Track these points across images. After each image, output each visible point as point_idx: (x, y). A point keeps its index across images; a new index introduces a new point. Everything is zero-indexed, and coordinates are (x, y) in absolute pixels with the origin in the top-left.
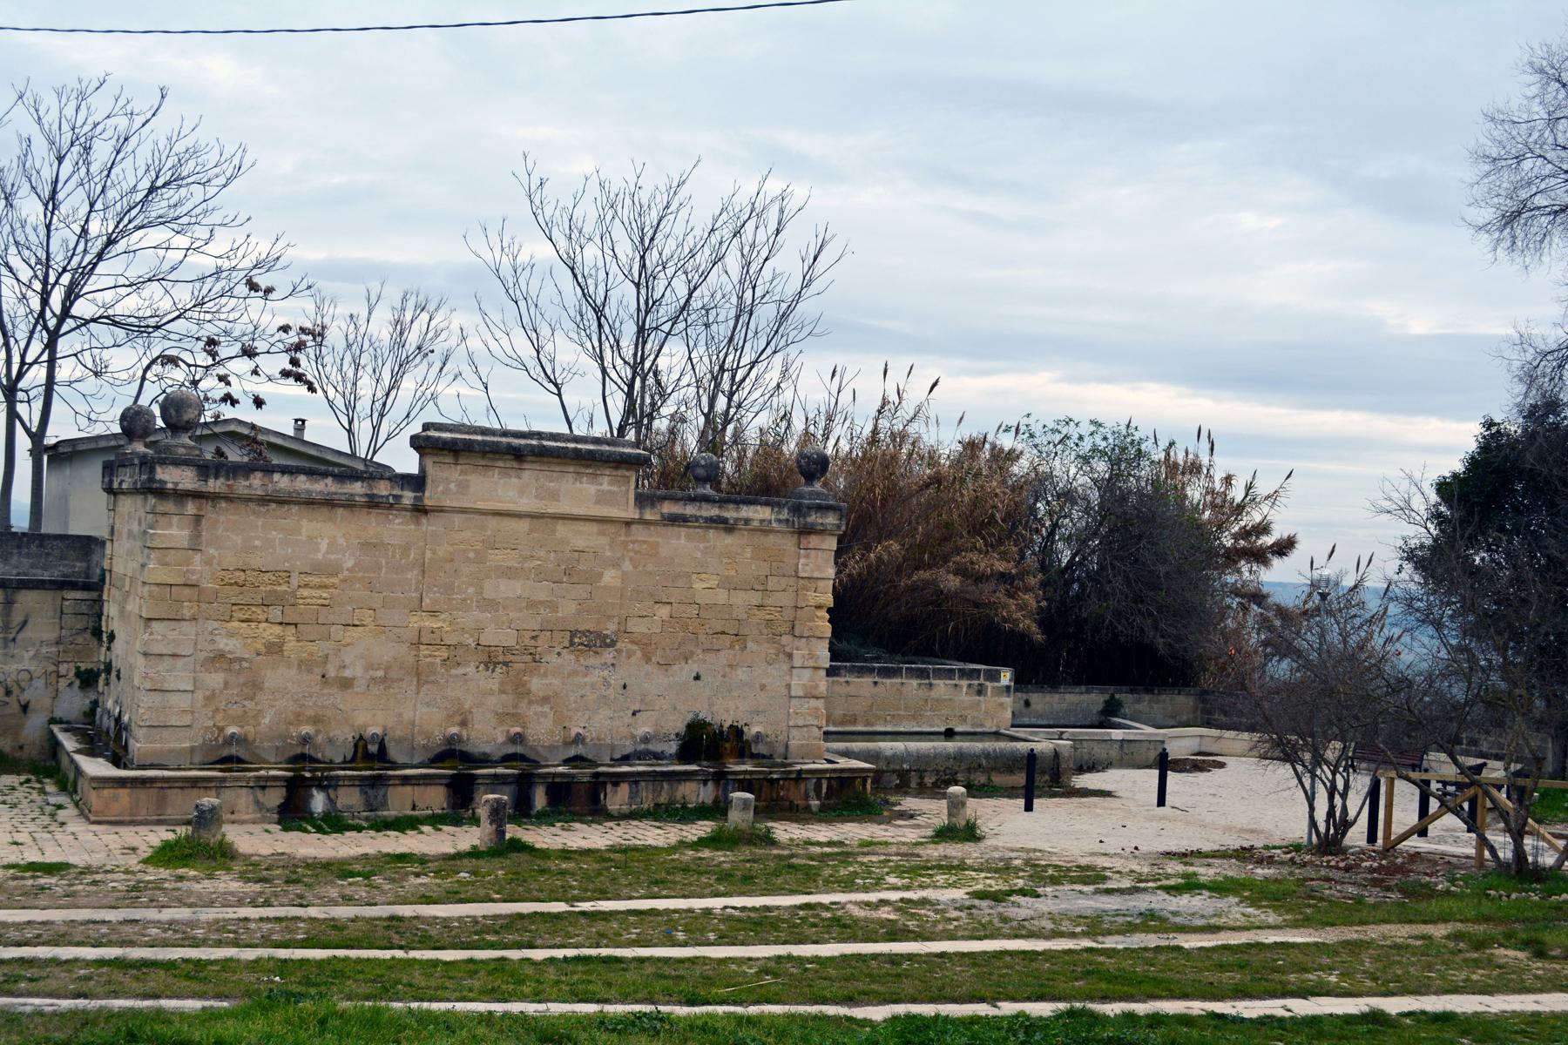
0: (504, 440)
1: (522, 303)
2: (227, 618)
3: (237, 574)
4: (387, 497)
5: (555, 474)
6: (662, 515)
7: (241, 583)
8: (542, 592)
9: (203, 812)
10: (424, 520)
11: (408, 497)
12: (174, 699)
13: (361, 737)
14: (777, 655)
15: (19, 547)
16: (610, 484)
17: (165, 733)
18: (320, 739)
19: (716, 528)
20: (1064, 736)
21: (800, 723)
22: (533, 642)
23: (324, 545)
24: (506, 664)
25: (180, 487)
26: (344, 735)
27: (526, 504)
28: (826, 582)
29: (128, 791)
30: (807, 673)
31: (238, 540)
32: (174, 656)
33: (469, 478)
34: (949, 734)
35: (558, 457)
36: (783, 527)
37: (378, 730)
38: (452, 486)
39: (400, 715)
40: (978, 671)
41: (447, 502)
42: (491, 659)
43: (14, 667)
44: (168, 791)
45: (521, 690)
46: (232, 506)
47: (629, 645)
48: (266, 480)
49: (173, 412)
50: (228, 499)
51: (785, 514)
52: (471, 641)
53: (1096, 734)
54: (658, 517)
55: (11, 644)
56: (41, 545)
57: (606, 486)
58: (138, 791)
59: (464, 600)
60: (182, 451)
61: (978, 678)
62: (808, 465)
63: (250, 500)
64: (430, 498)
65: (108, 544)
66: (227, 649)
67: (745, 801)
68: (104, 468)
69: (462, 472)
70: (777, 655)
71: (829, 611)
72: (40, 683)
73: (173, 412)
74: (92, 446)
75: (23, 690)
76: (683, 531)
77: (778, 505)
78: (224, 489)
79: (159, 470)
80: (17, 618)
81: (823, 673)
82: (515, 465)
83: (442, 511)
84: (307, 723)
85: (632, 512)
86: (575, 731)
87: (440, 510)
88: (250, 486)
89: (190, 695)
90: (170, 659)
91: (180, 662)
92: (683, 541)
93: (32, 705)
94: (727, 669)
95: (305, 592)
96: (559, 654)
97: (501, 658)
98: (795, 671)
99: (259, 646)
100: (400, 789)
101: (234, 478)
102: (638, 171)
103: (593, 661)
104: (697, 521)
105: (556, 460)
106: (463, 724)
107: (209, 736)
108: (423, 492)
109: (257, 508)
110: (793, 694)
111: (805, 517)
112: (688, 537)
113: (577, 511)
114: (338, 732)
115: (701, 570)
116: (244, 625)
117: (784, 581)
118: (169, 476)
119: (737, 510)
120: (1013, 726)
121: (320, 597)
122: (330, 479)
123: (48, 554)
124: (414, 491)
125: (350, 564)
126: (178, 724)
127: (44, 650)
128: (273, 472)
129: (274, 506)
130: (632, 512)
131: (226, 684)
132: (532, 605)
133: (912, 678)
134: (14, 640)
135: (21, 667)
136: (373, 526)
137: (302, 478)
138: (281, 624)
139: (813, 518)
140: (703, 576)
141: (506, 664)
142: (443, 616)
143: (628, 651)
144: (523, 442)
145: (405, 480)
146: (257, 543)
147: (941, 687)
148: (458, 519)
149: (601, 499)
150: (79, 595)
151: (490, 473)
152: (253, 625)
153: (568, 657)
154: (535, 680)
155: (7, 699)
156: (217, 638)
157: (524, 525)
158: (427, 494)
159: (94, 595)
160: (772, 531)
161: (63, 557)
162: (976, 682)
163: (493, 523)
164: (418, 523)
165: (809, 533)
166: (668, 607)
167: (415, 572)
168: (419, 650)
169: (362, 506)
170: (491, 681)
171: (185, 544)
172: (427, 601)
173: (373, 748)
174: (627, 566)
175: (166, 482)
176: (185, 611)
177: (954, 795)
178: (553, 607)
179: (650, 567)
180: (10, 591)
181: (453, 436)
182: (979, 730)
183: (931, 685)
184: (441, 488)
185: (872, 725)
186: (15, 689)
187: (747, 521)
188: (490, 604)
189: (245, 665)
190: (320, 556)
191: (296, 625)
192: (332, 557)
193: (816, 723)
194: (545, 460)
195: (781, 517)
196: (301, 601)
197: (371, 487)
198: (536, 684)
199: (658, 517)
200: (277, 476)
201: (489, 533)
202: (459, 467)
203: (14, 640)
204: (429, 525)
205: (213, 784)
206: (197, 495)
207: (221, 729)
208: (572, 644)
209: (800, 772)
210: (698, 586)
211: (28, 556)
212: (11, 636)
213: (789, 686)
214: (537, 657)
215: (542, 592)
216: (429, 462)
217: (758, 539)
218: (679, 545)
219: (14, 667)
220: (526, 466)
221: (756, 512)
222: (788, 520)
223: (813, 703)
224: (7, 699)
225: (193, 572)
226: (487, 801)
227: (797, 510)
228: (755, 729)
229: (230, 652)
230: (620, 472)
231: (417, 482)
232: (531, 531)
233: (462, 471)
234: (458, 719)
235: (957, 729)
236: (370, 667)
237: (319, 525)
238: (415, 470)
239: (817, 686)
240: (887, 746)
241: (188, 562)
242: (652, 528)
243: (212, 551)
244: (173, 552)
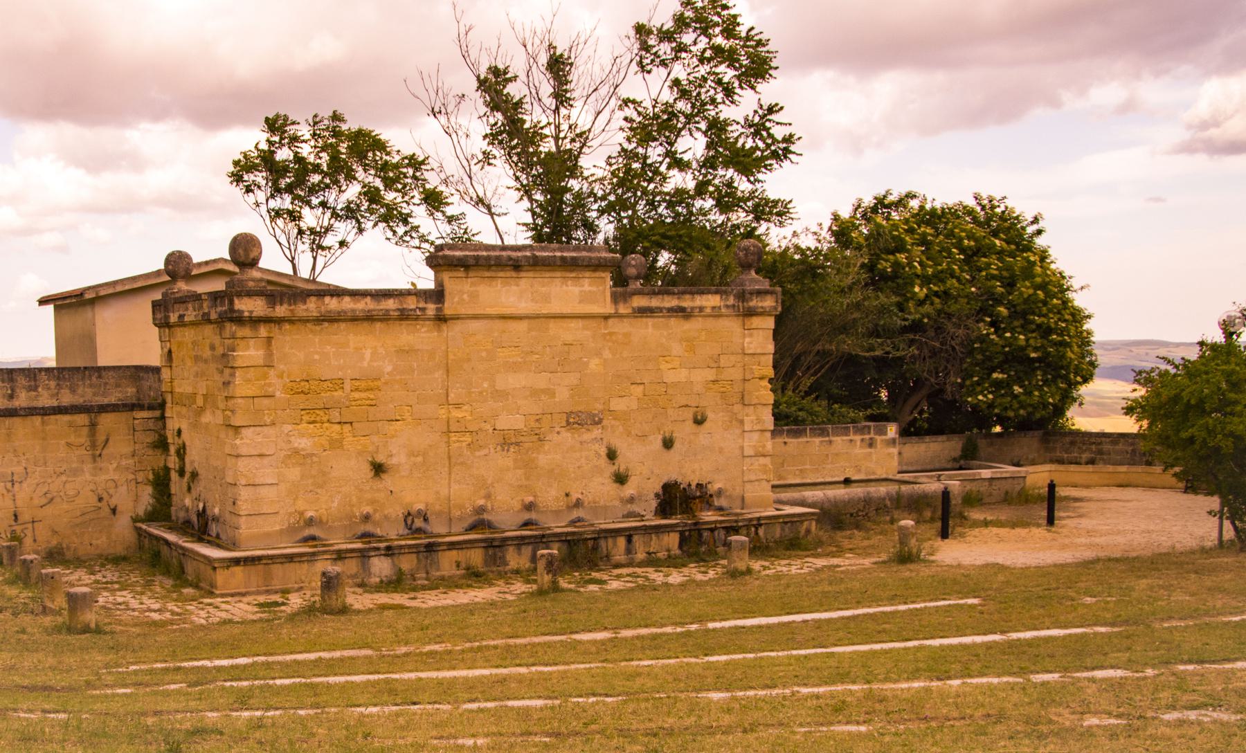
0: (504, 253)
1: (454, 136)
2: (298, 422)
3: (303, 384)
4: (415, 310)
5: (546, 280)
6: (633, 308)
7: (307, 391)
8: (541, 381)
9: (331, 578)
10: (444, 327)
11: (431, 308)
12: (264, 491)
13: (409, 514)
14: (731, 422)
15: (83, 379)
16: (590, 285)
17: (260, 519)
18: (377, 516)
19: (676, 317)
20: (942, 478)
21: (753, 477)
22: (537, 425)
23: (368, 354)
24: (517, 444)
25: (254, 314)
26: (397, 511)
27: (525, 307)
28: (767, 357)
29: (241, 568)
30: (756, 436)
31: (301, 355)
32: (261, 455)
33: (478, 289)
34: (847, 482)
35: (549, 265)
36: (730, 311)
37: (421, 506)
38: (465, 296)
39: (438, 493)
40: (869, 427)
41: (463, 311)
42: (507, 442)
43: (104, 477)
44: (272, 566)
45: (528, 466)
46: (295, 327)
47: (613, 422)
48: (320, 302)
49: (241, 251)
50: (291, 321)
51: (731, 301)
52: (489, 427)
53: (970, 475)
54: (630, 311)
55: (98, 459)
56: (100, 377)
57: (587, 288)
58: (248, 568)
59: (481, 393)
60: (251, 284)
61: (869, 433)
62: (746, 255)
63: (308, 321)
64: (449, 308)
65: (166, 374)
66: (301, 446)
67: (742, 543)
68: (154, 306)
69: (473, 284)
70: (731, 422)
71: (770, 381)
72: (123, 489)
73: (241, 251)
74: (111, 291)
75: (111, 496)
76: (650, 321)
77: (725, 292)
78: (288, 314)
79: (236, 301)
80: (101, 438)
81: (769, 435)
82: (514, 274)
83: (458, 318)
84: (367, 505)
85: (609, 309)
86: (575, 496)
87: (457, 318)
88: (307, 310)
89: (275, 487)
90: (258, 459)
91: (266, 461)
92: (650, 330)
93: (119, 509)
94: (692, 437)
95: (356, 395)
96: (558, 433)
97: (513, 440)
98: (746, 434)
99: (802, 394)
100: (448, 553)
101: (295, 303)
102: (555, 10)
103: (587, 436)
104: (661, 312)
105: (545, 268)
106: (488, 497)
108: (443, 303)
109: (313, 327)
110: (746, 454)
111: (747, 302)
112: (654, 326)
113: (567, 310)
114: (391, 510)
115: (666, 354)
116: (312, 426)
117: (733, 358)
118: (245, 306)
119: (693, 300)
120: (899, 473)
121: (369, 399)
122: (369, 298)
123: (106, 384)
124: (435, 303)
125: (389, 369)
126: (269, 511)
127: (124, 463)
128: (324, 295)
129: (326, 324)
130: (609, 309)
131: (302, 476)
132: (535, 393)
133: (815, 436)
134: (100, 455)
135: (107, 477)
136: (406, 336)
137: (347, 299)
138: (340, 423)
139: (754, 303)
140: (667, 358)
141: (517, 444)
142: (465, 407)
143: (612, 426)
144: (520, 254)
145: (425, 295)
146: (316, 357)
147: (839, 441)
148: (474, 325)
149: (585, 298)
150: (145, 414)
151: (494, 283)
152: (318, 425)
153: (566, 435)
154: (541, 456)
155: (99, 505)
156: (292, 439)
157: (523, 326)
158: (446, 305)
159: (157, 413)
160: (720, 316)
161: (118, 386)
162: (867, 437)
163: (499, 324)
164: (439, 330)
165: (751, 315)
166: (641, 387)
167: (441, 372)
168: (449, 438)
169: (396, 319)
170: (505, 460)
171: (261, 362)
172: (452, 395)
174: (607, 354)
175: (243, 312)
176: (266, 418)
177: (906, 528)
178: (551, 393)
179: (625, 354)
180: (93, 415)
181: (464, 253)
182: (872, 477)
183: (830, 442)
184: (456, 300)
185: (785, 479)
186: (105, 496)
187: (701, 309)
188: (501, 395)
189: (315, 459)
190: (365, 364)
191: (351, 423)
192: (375, 364)
193: (765, 477)
194: (538, 268)
195: (728, 303)
196: (353, 403)
197: (401, 303)
198: (543, 460)
199: (630, 311)
200: (327, 299)
201: (496, 334)
202: (469, 280)
203: (100, 455)
204: (454, 331)
205: (305, 558)
206: (267, 320)
207: (302, 513)
208: (568, 423)
209: (759, 519)
210: (664, 366)
211: (91, 386)
212: (98, 453)
213: (742, 448)
214: (542, 436)
215: (541, 381)
216: (446, 276)
217: (710, 323)
218: (648, 330)
219: (104, 477)
220: (523, 274)
221: (708, 300)
222: (734, 306)
223: (762, 460)
224: (99, 505)
225: (270, 385)
226: (543, 556)
227: (742, 296)
228: (716, 486)
229: (303, 449)
230: (597, 274)
231: (437, 295)
232: (530, 330)
233: (472, 283)
234: (483, 492)
235: (854, 478)
236: (412, 454)
237: (363, 338)
238: (431, 285)
239: (764, 446)
240: (809, 494)
241: (265, 377)
242: (625, 320)
243: (282, 367)
244: (252, 369)
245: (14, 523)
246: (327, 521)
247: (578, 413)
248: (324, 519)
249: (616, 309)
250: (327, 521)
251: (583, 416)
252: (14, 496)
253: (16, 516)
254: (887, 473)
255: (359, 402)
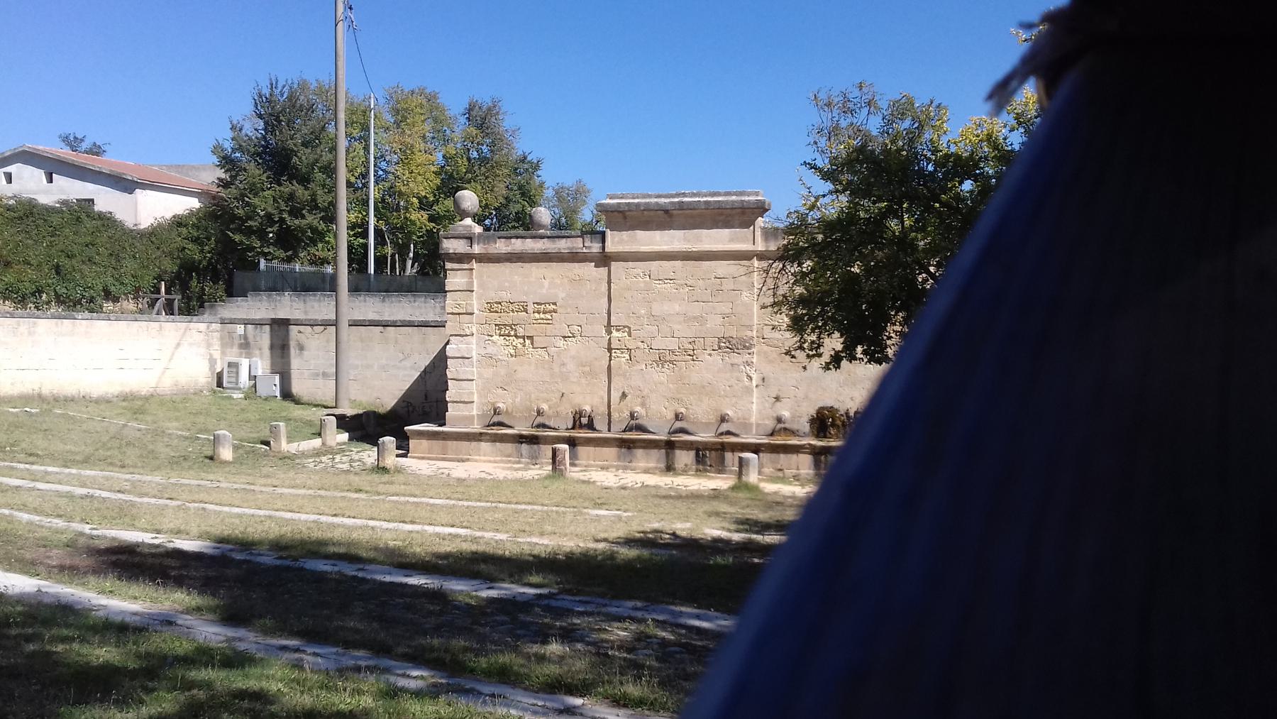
8: (696, 309)
24: (671, 362)
26: (567, 411)
60: (461, 228)
67: (736, 470)
96: (710, 355)
97: (668, 358)
101: (488, 243)
107: (485, 408)
132: (689, 319)
141: (671, 362)
144: (667, 200)
153: (717, 358)
173: (584, 421)
200: (513, 240)
215: (696, 309)
245: (424, 401)
246: (512, 412)
247: (729, 340)
248: (510, 410)
249: (767, 247)
250: (512, 412)
251: (734, 342)
252: (425, 382)
253: (426, 396)
254: (80, 324)
255: (539, 321)
